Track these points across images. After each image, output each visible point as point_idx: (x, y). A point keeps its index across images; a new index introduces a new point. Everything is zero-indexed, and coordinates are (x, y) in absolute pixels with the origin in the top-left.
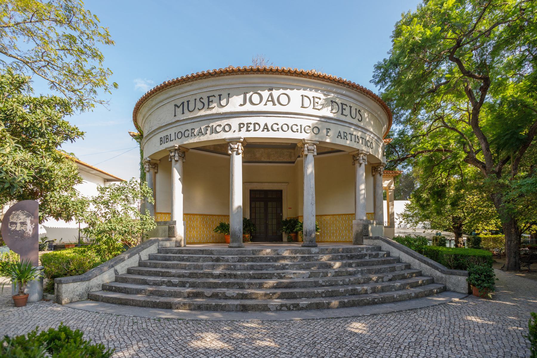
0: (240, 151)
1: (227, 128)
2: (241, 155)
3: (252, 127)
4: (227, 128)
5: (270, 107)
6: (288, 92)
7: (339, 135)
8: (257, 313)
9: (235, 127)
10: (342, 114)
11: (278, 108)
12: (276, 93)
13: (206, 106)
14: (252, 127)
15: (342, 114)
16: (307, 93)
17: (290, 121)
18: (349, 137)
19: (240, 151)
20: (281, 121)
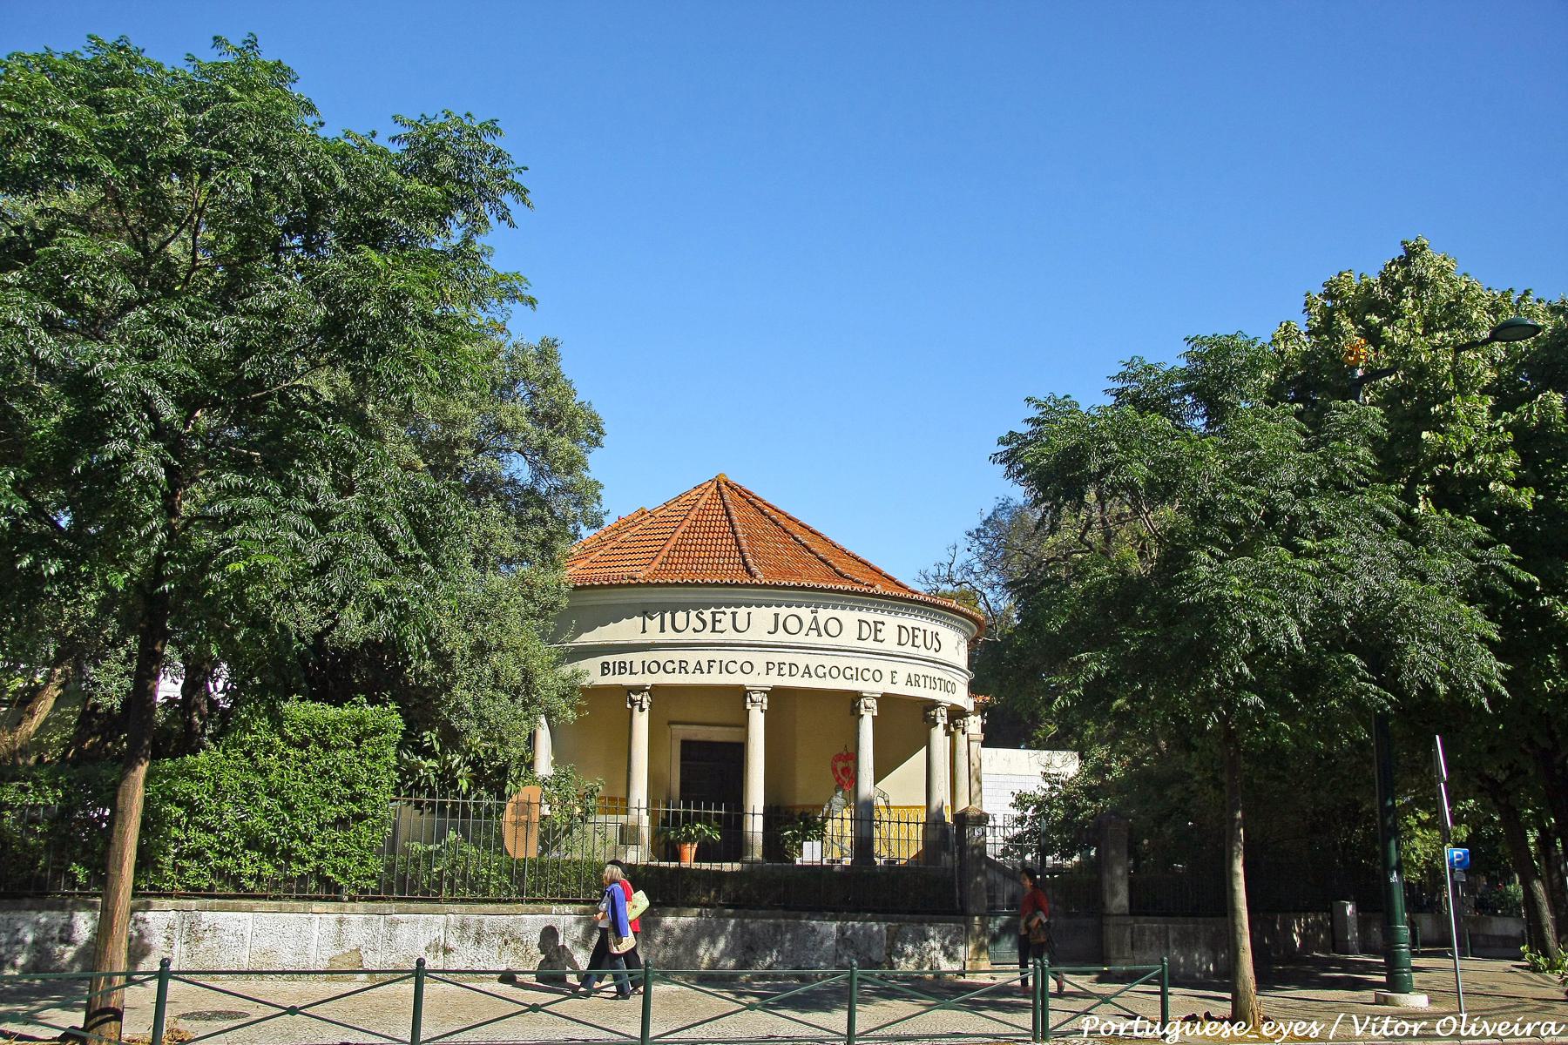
0: (645, 705)
1: (747, 668)
2: (646, 712)
3: (786, 669)
4: (747, 668)
5: (812, 640)
6: (838, 613)
7: (909, 681)
8: (620, 909)
9: (760, 666)
10: (876, 639)
11: (825, 641)
12: (824, 614)
13: (709, 626)
14: (786, 669)
15: (876, 639)
16: (864, 615)
17: (842, 662)
18: (922, 682)
19: (645, 705)
20: (829, 661)
